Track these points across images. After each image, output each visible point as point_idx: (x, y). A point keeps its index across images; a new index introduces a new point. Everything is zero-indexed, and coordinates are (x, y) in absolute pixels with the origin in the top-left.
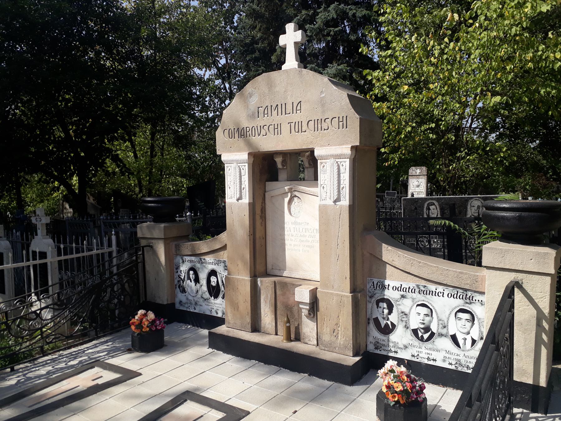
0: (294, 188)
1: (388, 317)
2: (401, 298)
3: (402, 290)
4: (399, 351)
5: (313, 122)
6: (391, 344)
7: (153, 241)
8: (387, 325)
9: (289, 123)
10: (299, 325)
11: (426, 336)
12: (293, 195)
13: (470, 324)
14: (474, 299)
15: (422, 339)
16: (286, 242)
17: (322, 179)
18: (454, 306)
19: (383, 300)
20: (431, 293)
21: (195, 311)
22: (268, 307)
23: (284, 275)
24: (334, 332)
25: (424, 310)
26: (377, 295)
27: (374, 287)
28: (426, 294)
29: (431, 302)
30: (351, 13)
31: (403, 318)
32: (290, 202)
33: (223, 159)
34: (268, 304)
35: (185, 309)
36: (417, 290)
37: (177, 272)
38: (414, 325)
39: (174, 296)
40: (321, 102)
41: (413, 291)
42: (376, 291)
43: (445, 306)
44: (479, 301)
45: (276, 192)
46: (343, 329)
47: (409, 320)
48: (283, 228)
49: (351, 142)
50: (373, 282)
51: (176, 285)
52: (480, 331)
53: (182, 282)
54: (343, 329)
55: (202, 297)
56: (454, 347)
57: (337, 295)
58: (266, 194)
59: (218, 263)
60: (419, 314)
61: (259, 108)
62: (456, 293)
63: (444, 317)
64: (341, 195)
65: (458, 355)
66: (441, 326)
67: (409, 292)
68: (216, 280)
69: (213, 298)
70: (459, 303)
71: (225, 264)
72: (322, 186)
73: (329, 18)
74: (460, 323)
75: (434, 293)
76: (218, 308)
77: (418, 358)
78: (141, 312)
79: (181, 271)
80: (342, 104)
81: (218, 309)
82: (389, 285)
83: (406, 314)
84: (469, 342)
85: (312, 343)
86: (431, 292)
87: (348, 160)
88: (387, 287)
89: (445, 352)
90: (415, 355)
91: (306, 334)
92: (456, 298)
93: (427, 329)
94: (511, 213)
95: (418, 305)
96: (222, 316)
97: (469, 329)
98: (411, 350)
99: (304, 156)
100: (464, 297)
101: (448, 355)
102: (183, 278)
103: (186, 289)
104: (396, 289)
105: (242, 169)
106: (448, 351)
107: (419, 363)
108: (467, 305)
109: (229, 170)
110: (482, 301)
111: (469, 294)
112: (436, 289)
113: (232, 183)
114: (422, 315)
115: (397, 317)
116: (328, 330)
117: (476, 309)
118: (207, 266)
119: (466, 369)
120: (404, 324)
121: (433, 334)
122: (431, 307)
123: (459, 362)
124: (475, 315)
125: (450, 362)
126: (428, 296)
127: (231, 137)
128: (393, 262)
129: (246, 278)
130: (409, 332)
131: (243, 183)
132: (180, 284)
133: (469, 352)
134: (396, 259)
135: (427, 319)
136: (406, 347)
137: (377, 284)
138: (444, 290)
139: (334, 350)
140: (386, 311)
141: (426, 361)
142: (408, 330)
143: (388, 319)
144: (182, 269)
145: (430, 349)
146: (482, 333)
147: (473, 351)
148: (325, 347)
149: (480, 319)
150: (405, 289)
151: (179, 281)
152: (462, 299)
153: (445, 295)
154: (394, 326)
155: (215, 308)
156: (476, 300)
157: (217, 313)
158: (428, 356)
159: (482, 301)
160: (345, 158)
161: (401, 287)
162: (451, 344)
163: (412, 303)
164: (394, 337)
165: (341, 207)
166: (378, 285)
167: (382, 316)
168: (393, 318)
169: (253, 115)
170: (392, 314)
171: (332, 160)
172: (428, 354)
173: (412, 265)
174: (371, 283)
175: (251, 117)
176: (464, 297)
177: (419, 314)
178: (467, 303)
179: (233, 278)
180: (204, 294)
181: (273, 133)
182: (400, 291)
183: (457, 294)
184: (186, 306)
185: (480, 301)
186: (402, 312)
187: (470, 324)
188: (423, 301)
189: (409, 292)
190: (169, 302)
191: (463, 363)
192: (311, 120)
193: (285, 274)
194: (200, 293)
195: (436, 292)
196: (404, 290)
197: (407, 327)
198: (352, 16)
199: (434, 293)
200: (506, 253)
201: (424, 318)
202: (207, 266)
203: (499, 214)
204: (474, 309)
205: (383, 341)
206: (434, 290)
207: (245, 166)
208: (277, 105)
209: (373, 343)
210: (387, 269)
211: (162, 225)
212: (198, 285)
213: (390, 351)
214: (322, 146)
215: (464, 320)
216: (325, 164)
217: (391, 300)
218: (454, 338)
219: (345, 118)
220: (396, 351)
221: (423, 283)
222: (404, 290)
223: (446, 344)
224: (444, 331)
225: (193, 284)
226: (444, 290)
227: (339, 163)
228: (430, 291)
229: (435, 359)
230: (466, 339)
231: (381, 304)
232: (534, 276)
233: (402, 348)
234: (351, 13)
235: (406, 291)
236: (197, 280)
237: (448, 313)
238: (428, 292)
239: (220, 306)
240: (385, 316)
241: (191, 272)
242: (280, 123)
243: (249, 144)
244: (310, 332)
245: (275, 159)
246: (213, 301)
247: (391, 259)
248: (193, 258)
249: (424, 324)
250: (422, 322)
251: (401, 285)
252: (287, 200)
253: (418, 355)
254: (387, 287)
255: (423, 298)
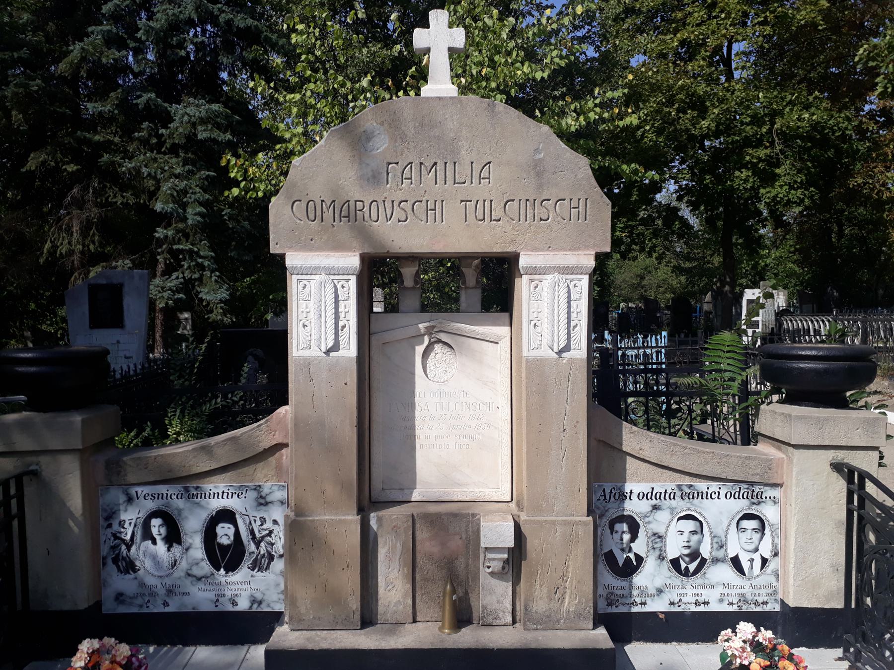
0: (439, 325)
1: (630, 546)
2: (652, 511)
3: (653, 497)
4: (649, 601)
5: (516, 203)
6: (635, 592)
7: (44, 460)
8: (628, 560)
9: (462, 201)
10: (467, 593)
11: (692, 567)
12: (432, 340)
13: (758, 535)
14: (763, 497)
15: (686, 573)
16: (418, 432)
17: (534, 310)
18: (736, 511)
19: (622, 519)
20: (701, 495)
21: (167, 610)
22: (396, 571)
23: (413, 499)
24: (556, 593)
25: (690, 525)
26: (611, 511)
27: (605, 498)
28: (693, 498)
29: (700, 510)
30: (223, 18)
31: (656, 543)
32: (426, 354)
33: (288, 262)
34: (397, 562)
35: (135, 610)
36: (678, 494)
37: (110, 526)
38: (672, 554)
39: (99, 584)
40: (535, 169)
41: (672, 497)
42: (609, 505)
43: (721, 513)
44: (770, 498)
45: (399, 334)
46: (574, 584)
47: (665, 545)
48: (411, 406)
49: (594, 245)
50: (604, 490)
51: (104, 558)
52: (773, 544)
53: (124, 547)
54: (574, 584)
55: (189, 575)
56: (640, 575)
57: (566, 523)
58: (373, 338)
59: (240, 491)
60: (681, 533)
61: (390, 163)
62: (738, 490)
63: (720, 532)
64: (572, 339)
65: (741, 587)
66: (716, 546)
67: (665, 498)
68: (231, 531)
69: (222, 571)
70: (741, 506)
71: (259, 492)
72: (533, 323)
73: (181, 16)
74: (744, 536)
75: (705, 495)
76: (238, 592)
77: (679, 606)
78: (86, 646)
79: (121, 524)
80: (580, 176)
81: (236, 595)
82: (631, 491)
83: (660, 537)
84: (758, 563)
85: (503, 622)
86: (700, 494)
87: (587, 276)
88: (628, 495)
89: (722, 586)
90: (676, 602)
91: (489, 607)
92: (739, 498)
93: (694, 555)
94: (819, 364)
95: (680, 519)
96: (251, 607)
97: (757, 544)
98: (668, 594)
99: (469, 266)
100: (750, 495)
101: (726, 591)
102: (128, 537)
103: (138, 563)
104: (643, 496)
105: (339, 286)
106: (726, 585)
107: (682, 614)
108: (754, 507)
109: (304, 288)
110: (774, 498)
111: (757, 489)
112: (708, 488)
113: (311, 316)
114: (686, 534)
115: (645, 542)
116: (545, 590)
117: (769, 512)
118: (203, 502)
119: (753, 606)
120: (657, 553)
121: (703, 561)
122: (700, 518)
123: (743, 599)
124: (765, 521)
125: (731, 601)
126: (696, 501)
127: (312, 216)
128: (641, 452)
129: (350, 518)
130: (666, 565)
131: (342, 315)
132: (118, 554)
133: (758, 579)
134: (646, 445)
135: (695, 538)
136: (660, 591)
137: (611, 492)
138: (720, 488)
139: (556, 626)
140: (627, 537)
141: (693, 608)
142: (665, 562)
143: (630, 550)
144: (124, 516)
145: (700, 586)
146: (776, 547)
147: (763, 576)
148: (538, 623)
149: (772, 525)
150: (658, 494)
151: (114, 548)
152: (747, 498)
153: (722, 496)
154: (640, 559)
155: (229, 594)
156: (766, 498)
157: (234, 603)
158: (697, 598)
159: (774, 498)
160: (581, 274)
161: (652, 493)
162: (731, 571)
163: (670, 517)
164: (640, 579)
165: (571, 361)
166: (613, 495)
167: (620, 547)
168: (639, 547)
169: (374, 177)
170: (637, 541)
171: (322, 277)
172: (697, 595)
173: (672, 454)
174: (600, 492)
175: (368, 180)
176: (750, 495)
177: (681, 533)
178: (754, 503)
179: (313, 521)
180: (194, 568)
181: (424, 219)
182: (651, 498)
183: (739, 492)
184: (139, 601)
185: (772, 498)
186: (654, 534)
187: (758, 535)
188: (689, 510)
189: (665, 498)
190: (91, 603)
191: (749, 597)
192: (513, 200)
193: (416, 496)
194: (183, 565)
195: (707, 493)
196: (658, 497)
197: (661, 558)
198: (224, 23)
199: (705, 495)
200: (825, 422)
201: (689, 538)
202: (203, 502)
203: (794, 365)
204: (763, 511)
205: (622, 588)
206: (704, 490)
207: (348, 280)
208: (435, 164)
209: (605, 596)
210: (628, 466)
211: (77, 419)
212: (177, 549)
213: (634, 604)
214: (535, 249)
215: (749, 531)
216: (307, 283)
217: (635, 516)
218: (736, 562)
219: (582, 203)
220: (643, 601)
221: (687, 481)
222: (658, 497)
223: (723, 573)
224: (720, 554)
225: (161, 548)
226: (720, 488)
227: (336, 282)
228: (698, 493)
229: (707, 601)
230: (753, 560)
231: (618, 527)
232: (858, 452)
233: (653, 595)
234: (223, 18)
235: (660, 498)
236: (173, 537)
237: (726, 523)
238: (696, 494)
239: (245, 587)
240: (625, 546)
241: (156, 522)
242: (442, 198)
243: (363, 234)
244: (498, 602)
245: (401, 270)
246: (223, 580)
247: (638, 447)
248: (163, 489)
249: (689, 547)
250: (686, 544)
251: (653, 489)
252: (420, 350)
253: (680, 600)
254: (628, 495)
255: (688, 505)
